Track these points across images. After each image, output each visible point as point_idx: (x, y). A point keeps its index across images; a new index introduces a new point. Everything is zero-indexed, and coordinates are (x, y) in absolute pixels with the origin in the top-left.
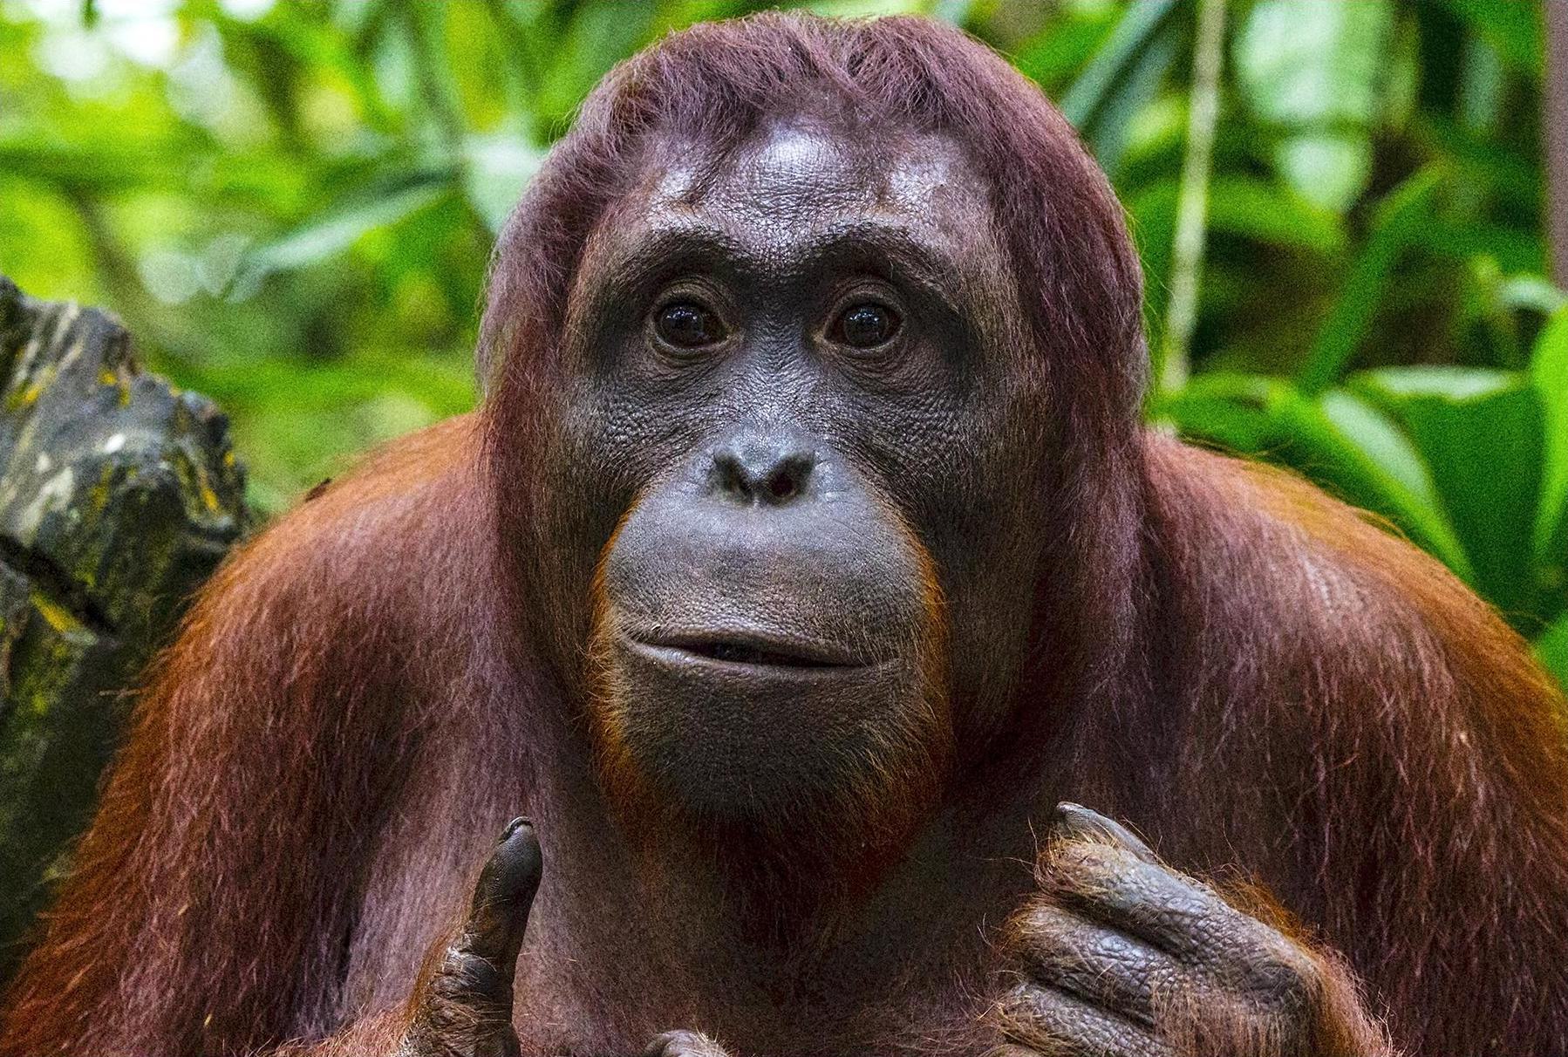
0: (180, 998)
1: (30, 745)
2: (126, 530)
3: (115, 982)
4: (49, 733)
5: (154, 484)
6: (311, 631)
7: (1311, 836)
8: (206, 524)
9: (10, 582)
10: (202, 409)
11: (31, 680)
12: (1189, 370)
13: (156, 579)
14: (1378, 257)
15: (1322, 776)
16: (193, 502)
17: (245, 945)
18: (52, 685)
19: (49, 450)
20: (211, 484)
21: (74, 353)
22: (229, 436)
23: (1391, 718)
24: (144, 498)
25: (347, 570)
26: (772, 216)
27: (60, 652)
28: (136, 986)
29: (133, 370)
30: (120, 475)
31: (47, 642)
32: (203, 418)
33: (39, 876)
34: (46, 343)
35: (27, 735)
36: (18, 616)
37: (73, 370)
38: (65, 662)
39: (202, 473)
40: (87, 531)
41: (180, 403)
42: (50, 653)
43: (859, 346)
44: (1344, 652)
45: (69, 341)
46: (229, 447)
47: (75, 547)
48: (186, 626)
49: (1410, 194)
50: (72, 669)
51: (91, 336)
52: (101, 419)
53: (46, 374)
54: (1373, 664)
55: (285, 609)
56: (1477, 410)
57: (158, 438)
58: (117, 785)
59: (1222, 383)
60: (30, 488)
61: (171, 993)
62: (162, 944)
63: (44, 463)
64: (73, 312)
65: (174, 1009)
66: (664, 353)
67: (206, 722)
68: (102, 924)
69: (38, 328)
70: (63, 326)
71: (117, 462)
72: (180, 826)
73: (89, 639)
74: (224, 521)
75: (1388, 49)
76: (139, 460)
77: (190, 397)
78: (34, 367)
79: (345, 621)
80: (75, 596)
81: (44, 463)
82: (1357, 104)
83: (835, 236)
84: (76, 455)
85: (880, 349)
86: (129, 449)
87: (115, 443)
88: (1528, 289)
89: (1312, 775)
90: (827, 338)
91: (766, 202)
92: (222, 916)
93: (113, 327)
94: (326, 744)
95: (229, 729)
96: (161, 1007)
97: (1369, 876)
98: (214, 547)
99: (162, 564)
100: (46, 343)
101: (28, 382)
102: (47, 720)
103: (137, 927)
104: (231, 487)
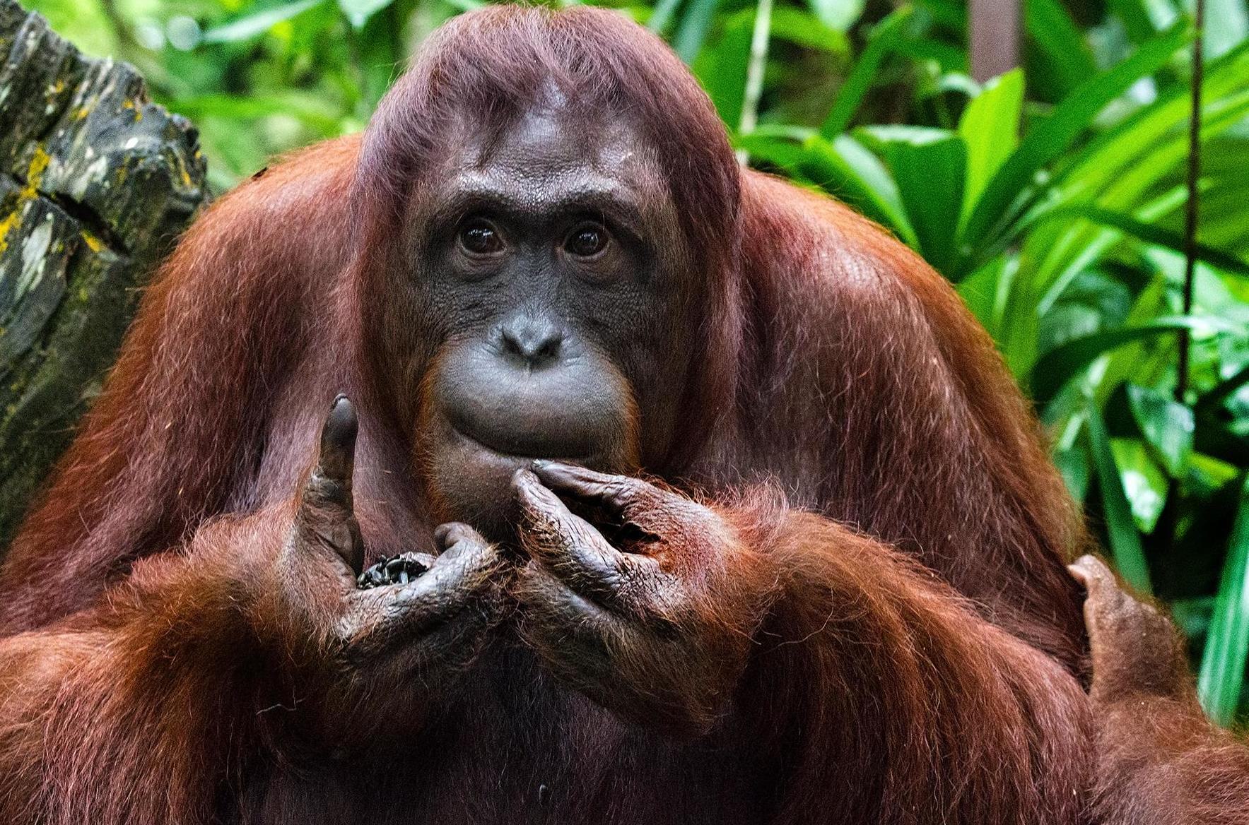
1: (78, 318)
2: (137, 194)
6: (249, 264)
8: (183, 193)
10: (183, 125)
11: (79, 281)
12: (756, 121)
13: (155, 223)
16: (177, 179)
17: (204, 448)
18: (91, 283)
19: (92, 145)
21: (109, 89)
24: (148, 176)
25: (271, 229)
26: (531, 178)
27: (96, 264)
29: (143, 100)
30: (134, 162)
31: (89, 258)
32: (184, 130)
34: (93, 83)
35: (75, 312)
36: (72, 243)
37: (108, 100)
38: (99, 271)
39: (182, 162)
41: (170, 121)
42: (91, 264)
43: (584, 255)
44: (866, 308)
45: (106, 82)
46: (198, 148)
47: (107, 204)
50: (104, 276)
52: (124, 129)
53: (93, 102)
56: (926, 151)
57: (158, 141)
58: (132, 347)
59: (772, 129)
60: (82, 166)
61: (160, 473)
63: (90, 153)
64: (109, 65)
66: (465, 255)
67: (186, 315)
69: (89, 73)
70: (103, 73)
71: (133, 154)
72: (169, 374)
73: (114, 257)
74: (194, 191)
76: (144, 154)
77: (176, 118)
78: (85, 96)
81: (90, 153)
83: (571, 200)
84: (110, 149)
85: (595, 257)
86: (141, 147)
90: (565, 249)
91: (526, 169)
92: (191, 428)
93: (133, 75)
94: (255, 332)
95: (199, 319)
98: (189, 206)
99: (158, 215)
100: (93, 83)
101: (82, 105)
102: (87, 305)
103: (141, 432)
104: (199, 171)
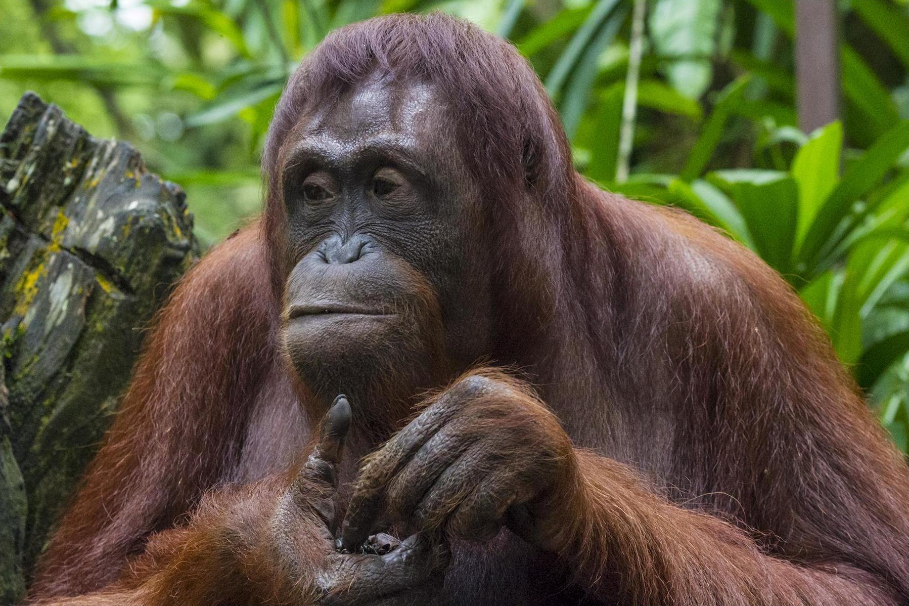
0: (168, 470)
3: (138, 464)
4: (104, 341)
5: (152, 224)
6: (228, 299)
7: (686, 379)
8: (176, 243)
9: (85, 270)
10: (174, 189)
11: (95, 316)
13: (153, 269)
14: (719, 118)
15: (691, 352)
16: (170, 232)
17: (197, 446)
18: (105, 318)
20: (178, 225)
21: (114, 163)
22: (187, 201)
23: (722, 322)
24: (147, 231)
27: (109, 303)
28: (148, 465)
29: (141, 171)
30: (136, 220)
31: (103, 298)
32: (174, 193)
33: (99, 408)
35: (93, 341)
36: (89, 286)
37: (113, 172)
38: (111, 308)
39: (174, 219)
40: (121, 246)
41: (164, 186)
45: (112, 157)
47: (115, 254)
48: (172, 298)
49: (733, 89)
50: (115, 312)
51: (123, 154)
52: (127, 194)
53: (101, 174)
54: (714, 297)
55: (216, 290)
57: (154, 203)
60: (94, 226)
62: (159, 446)
63: (100, 214)
65: (166, 476)
68: (132, 436)
69: (97, 152)
70: (109, 150)
71: (134, 214)
73: (122, 297)
74: (185, 242)
75: (720, 20)
76: (144, 213)
78: (95, 170)
79: (242, 296)
80: (115, 277)
81: (100, 214)
82: (706, 46)
84: (116, 211)
86: (141, 208)
87: (133, 205)
88: (788, 133)
89: (686, 350)
94: (234, 353)
96: (160, 476)
97: (712, 399)
99: (156, 261)
101: (93, 176)
102: (103, 335)
103: (148, 438)
104: (187, 225)
